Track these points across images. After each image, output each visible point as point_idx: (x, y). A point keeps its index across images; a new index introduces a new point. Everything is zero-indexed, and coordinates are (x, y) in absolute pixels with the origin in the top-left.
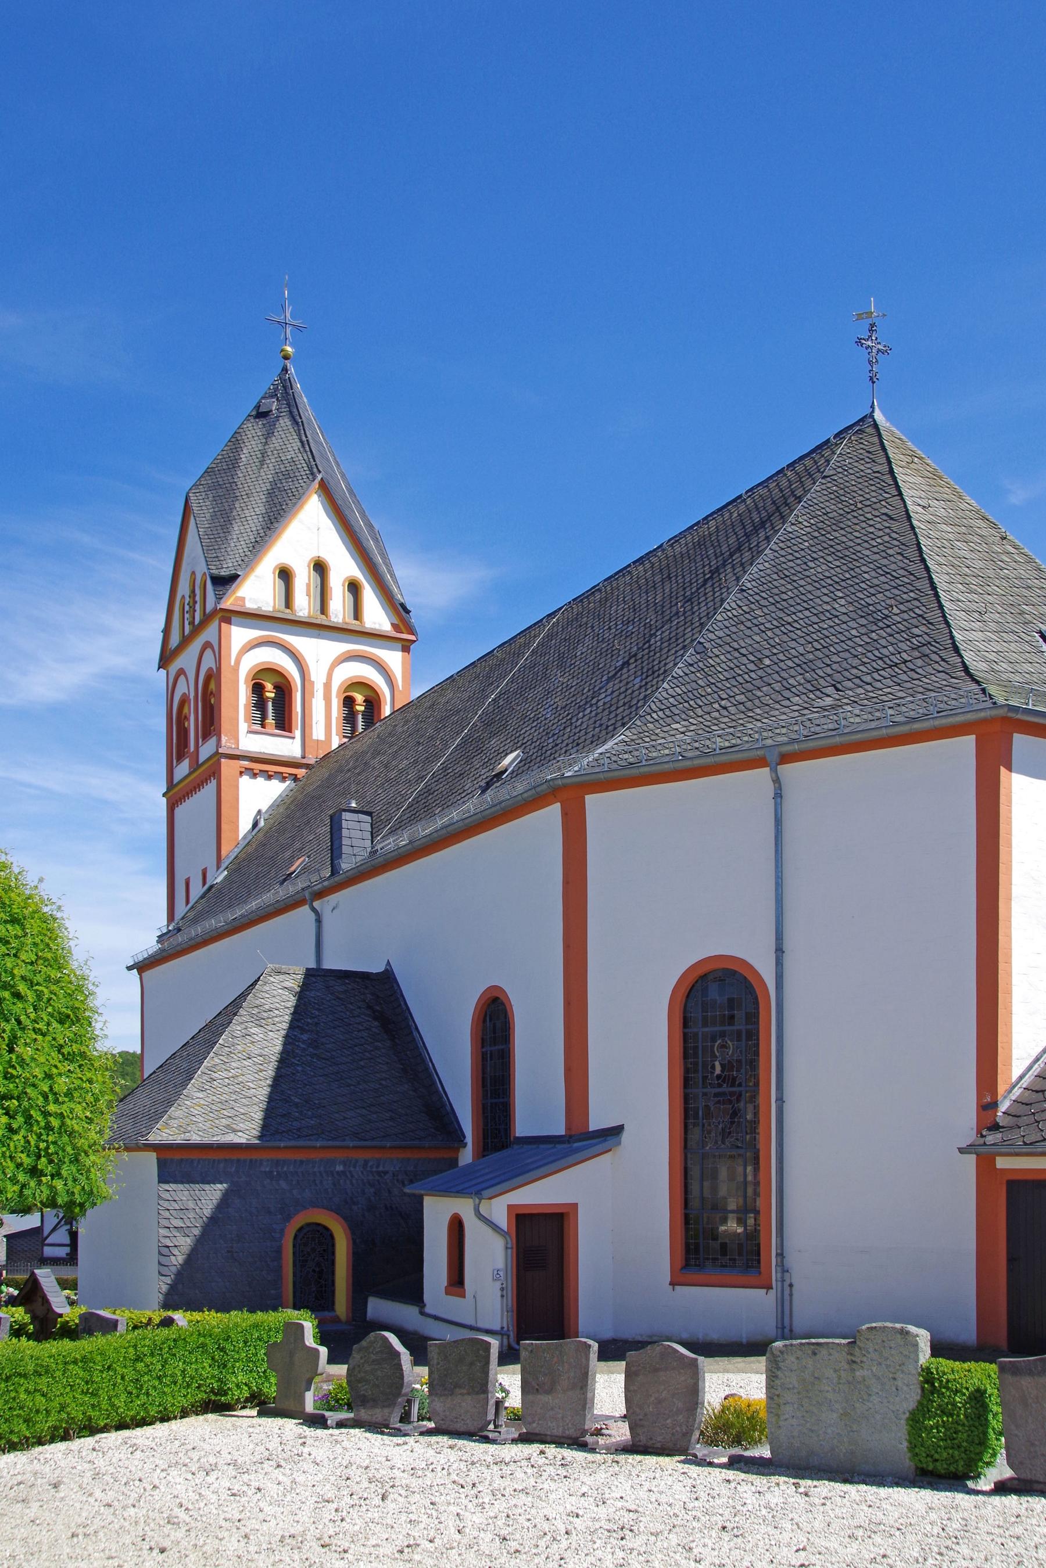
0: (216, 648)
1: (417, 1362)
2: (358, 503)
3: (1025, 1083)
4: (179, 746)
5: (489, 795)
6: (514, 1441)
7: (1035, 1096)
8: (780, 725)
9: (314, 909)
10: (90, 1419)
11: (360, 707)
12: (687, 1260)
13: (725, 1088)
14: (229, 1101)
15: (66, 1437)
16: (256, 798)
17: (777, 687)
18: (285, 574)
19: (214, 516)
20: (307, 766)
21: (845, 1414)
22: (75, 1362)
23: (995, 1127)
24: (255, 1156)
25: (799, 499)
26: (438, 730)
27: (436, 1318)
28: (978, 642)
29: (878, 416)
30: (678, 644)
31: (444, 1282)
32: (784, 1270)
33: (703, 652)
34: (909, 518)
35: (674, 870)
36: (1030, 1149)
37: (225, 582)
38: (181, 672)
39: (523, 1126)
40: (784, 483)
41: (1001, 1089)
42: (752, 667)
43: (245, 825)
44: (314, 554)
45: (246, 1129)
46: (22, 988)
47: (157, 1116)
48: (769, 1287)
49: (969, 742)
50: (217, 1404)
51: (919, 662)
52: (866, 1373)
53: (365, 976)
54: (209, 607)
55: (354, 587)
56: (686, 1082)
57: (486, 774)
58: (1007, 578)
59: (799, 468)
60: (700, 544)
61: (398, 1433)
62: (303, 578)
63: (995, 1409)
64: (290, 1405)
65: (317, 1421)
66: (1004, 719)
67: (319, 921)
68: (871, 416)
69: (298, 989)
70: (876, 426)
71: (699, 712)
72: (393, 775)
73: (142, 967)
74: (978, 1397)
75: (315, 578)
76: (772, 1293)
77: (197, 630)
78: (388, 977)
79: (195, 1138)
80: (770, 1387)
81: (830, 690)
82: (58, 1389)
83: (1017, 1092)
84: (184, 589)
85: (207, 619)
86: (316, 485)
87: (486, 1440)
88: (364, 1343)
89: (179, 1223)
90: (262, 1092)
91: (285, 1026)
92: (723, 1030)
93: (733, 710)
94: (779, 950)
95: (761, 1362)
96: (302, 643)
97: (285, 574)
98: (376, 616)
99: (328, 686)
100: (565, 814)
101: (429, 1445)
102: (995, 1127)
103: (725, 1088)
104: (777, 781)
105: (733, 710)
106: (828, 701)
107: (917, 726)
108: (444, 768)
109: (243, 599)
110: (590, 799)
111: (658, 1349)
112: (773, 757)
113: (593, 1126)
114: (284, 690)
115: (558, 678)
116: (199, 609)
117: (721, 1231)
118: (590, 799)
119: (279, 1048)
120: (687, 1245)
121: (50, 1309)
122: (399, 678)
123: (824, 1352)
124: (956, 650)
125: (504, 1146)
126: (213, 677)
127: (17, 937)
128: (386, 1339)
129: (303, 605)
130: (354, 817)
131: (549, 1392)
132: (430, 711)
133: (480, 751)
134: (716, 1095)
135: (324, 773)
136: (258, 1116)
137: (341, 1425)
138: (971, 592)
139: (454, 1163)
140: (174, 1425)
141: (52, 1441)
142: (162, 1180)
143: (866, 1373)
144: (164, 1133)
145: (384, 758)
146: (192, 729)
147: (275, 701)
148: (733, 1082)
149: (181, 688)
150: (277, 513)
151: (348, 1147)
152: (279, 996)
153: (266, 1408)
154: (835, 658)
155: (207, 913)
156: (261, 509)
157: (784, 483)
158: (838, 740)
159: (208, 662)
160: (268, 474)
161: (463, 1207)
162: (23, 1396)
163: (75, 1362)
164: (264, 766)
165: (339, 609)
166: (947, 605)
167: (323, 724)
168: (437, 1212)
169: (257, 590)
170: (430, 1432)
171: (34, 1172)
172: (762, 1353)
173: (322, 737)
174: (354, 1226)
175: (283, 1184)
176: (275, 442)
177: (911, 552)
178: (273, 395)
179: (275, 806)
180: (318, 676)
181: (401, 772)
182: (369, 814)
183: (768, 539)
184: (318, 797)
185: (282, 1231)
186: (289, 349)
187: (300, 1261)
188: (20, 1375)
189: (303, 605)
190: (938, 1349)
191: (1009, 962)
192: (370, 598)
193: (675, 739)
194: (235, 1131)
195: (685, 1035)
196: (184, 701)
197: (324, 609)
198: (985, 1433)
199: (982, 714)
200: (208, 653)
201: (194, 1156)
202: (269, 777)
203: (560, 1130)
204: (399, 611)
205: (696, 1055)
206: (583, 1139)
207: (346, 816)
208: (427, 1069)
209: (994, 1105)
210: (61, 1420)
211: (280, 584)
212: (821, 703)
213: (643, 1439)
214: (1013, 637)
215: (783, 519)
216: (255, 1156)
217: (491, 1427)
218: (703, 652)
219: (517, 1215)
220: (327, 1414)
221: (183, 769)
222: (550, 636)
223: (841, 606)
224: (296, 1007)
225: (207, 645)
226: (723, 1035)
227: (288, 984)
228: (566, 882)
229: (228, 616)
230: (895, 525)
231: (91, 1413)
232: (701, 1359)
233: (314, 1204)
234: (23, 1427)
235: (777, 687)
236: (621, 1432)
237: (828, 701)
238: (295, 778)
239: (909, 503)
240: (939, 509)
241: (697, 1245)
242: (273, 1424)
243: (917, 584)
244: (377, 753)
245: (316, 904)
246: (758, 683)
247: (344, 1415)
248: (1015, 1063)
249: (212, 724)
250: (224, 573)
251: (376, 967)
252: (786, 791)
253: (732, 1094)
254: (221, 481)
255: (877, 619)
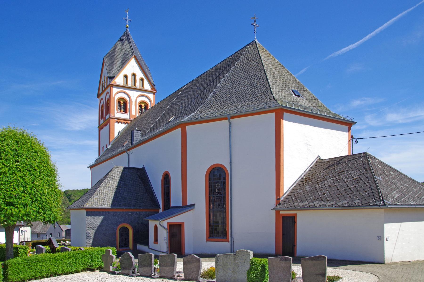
0: (109, 93)
1: (135, 259)
2: (143, 61)
3: (287, 194)
4: (101, 116)
5: (167, 126)
6: (158, 278)
7: (289, 197)
8: (232, 110)
9: (127, 153)
10: (57, 272)
11: (143, 107)
12: (210, 235)
13: (219, 195)
14: (104, 198)
15: (51, 276)
16: (118, 128)
17: (231, 101)
18: (126, 76)
19: (110, 63)
20: (131, 121)
21: (233, 271)
22: (52, 259)
23: (280, 204)
24: (110, 211)
25: (238, 59)
26: (158, 112)
27: (152, 249)
28: (276, 92)
29: (256, 41)
30: (210, 91)
31: (153, 241)
32: (232, 238)
33: (215, 93)
34: (262, 63)
35: (207, 144)
36: (287, 209)
37: (112, 78)
38: (102, 99)
39: (173, 204)
40: (235, 55)
41: (281, 195)
42: (226, 97)
43: (116, 134)
44: (133, 72)
45: (108, 205)
46: (36, 168)
47: (86, 201)
48: (229, 242)
49: (274, 114)
50: (90, 269)
51: (263, 96)
52: (238, 261)
53: (138, 169)
54: (108, 84)
55: (142, 80)
56: (210, 194)
57: (167, 122)
58: (285, 78)
59: (239, 52)
60: (217, 70)
61: (132, 276)
62: (130, 77)
63: (267, 269)
64: (107, 269)
65: (113, 273)
66: (281, 109)
67: (129, 156)
68: (255, 41)
69: (121, 171)
70: (256, 43)
71: (213, 107)
72: (148, 122)
73: (91, 167)
74: (263, 266)
75: (133, 77)
76: (229, 243)
77: (106, 89)
78: (143, 169)
79: (95, 206)
80: (216, 265)
81: (243, 102)
82: (48, 265)
83: (285, 196)
84: (103, 80)
85: (108, 86)
86: (133, 56)
87: (152, 278)
88: (124, 255)
89: (91, 227)
90: (112, 195)
91: (118, 180)
92: (218, 181)
93: (221, 106)
94: (231, 163)
95: (214, 259)
96: (130, 92)
97: (126, 76)
98: (147, 86)
99: (136, 102)
100: (182, 130)
101: (137, 279)
102: (280, 204)
103: (219, 195)
104: (230, 123)
105: (221, 106)
106: (242, 104)
107: (262, 110)
108: (158, 121)
109: (116, 82)
110: (188, 127)
111: (191, 256)
112: (229, 117)
113: (188, 204)
114: (125, 103)
115: (184, 100)
116: (106, 84)
117: (218, 229)
118: (188, 127)
119: (116, 185)
120: (210, 232)
121: (54, 246)
122: (151, 99)
123: (228, 256)
124: (272, 93)
125: (169, 209)
126: (109, 100)
127: (36, 156)
128: (128, 254)
129: (130, 84)
130: (137, 131)
131: (166, 266)
132: (158, 107)
133: (166, 116)
134: (217, 197)
135: (134, 122)
136: (111, 201)
137: (118, 274)
138: (276, 80)
139: (158, 212)
140: (79, 274)
141: (47, 277)
142: (87, 215)
143: (238, 261)
144: (88, 205)
145: (147, 119)
146: (105, 111)
147: (123, 105)
148: (220, 193)
149: (102, 103)
150: (124, 62)
151: (132, 209)
152: (117, 173)
153: (102, 270)
154: (244, 95)
155: (106, 155)
156: (120, 62)
157: (235, 55)
158: (243, 113)
159: (108, 96)
160: (122, 54)
161: (157, 223)
162: (39, 267)
163: (52, 259)
164: (120, 121)
165: (138, 84)
166: (270, 83)
167: (135, 111)
168: (152, 224)
169: (119, 80)
170: (139, 276)
171: (38, 212)
172: (214, 257)
173: (134, 114)
174: (134, 228)
175: (116, 217)
176: (124, 46)
177: (262, 71)
178: (124, 36)
179: (123, 130)
180: (133, 100)
181: (150, 122)
182: (140, 131)
183: (231, 68)
184: (132, 126)
185: (116, 229)
186: (128, 26)
187: (121, 236)
188: (38, 262)
189: (130, 84)
190: (255, 256)
191: (283, 165)
192: (146, 82)
193: (207, 113)
194: (105, 205)
195: (209, 183)
196: (102, 106)
197: (135, 85)
198: (265, 275)
199: (276, 108)
200: (108, 94)
201: (95, 211)
202: (122, 123)
203: (181, 205)
204: (153, 86)
205: (212, 187)
206: (186, 207)
207: (135, 131)
208: (152, 190)
209: (280, 199)
210: (49, 272)
211: (141, 82)
212: (240, 105)
213: (188, 277)
214: (285, 91)
215: (234, 63)
216: (110, 211)
217: (153, 274)
218: (215, 93)
219: (170, 225)
220: (116, 271)
221: (102, 121)
222: (184, 91)
223: (246, 83)
224: (121, 176)
225: (108, 93)
226: (218, 182)
227: (119, 170)
228: (182, 146)
229: (113, 86)
230: (259, 65)
231: (57, 271)
232: (200, 258)
233: (124, 222)
234: (39, 274)
235: (231, 101)
236: (183, 276)
237: (242, 104)
238: (128, 123)
239: (262, 60)
240: (270, 62)
241: (212, 232)
242: (102, 273)
243: (264, 78)
244: (145, 117)
245: (128, 152)
246: (227, 100)
247: (118, 272)
248: (284, 189)
249: (108, 111)
250: (111, 76)
251: (141, 167)
252: (232, 125)
253: (220, 196)
254: (112, 55)
255: (254, 86)
